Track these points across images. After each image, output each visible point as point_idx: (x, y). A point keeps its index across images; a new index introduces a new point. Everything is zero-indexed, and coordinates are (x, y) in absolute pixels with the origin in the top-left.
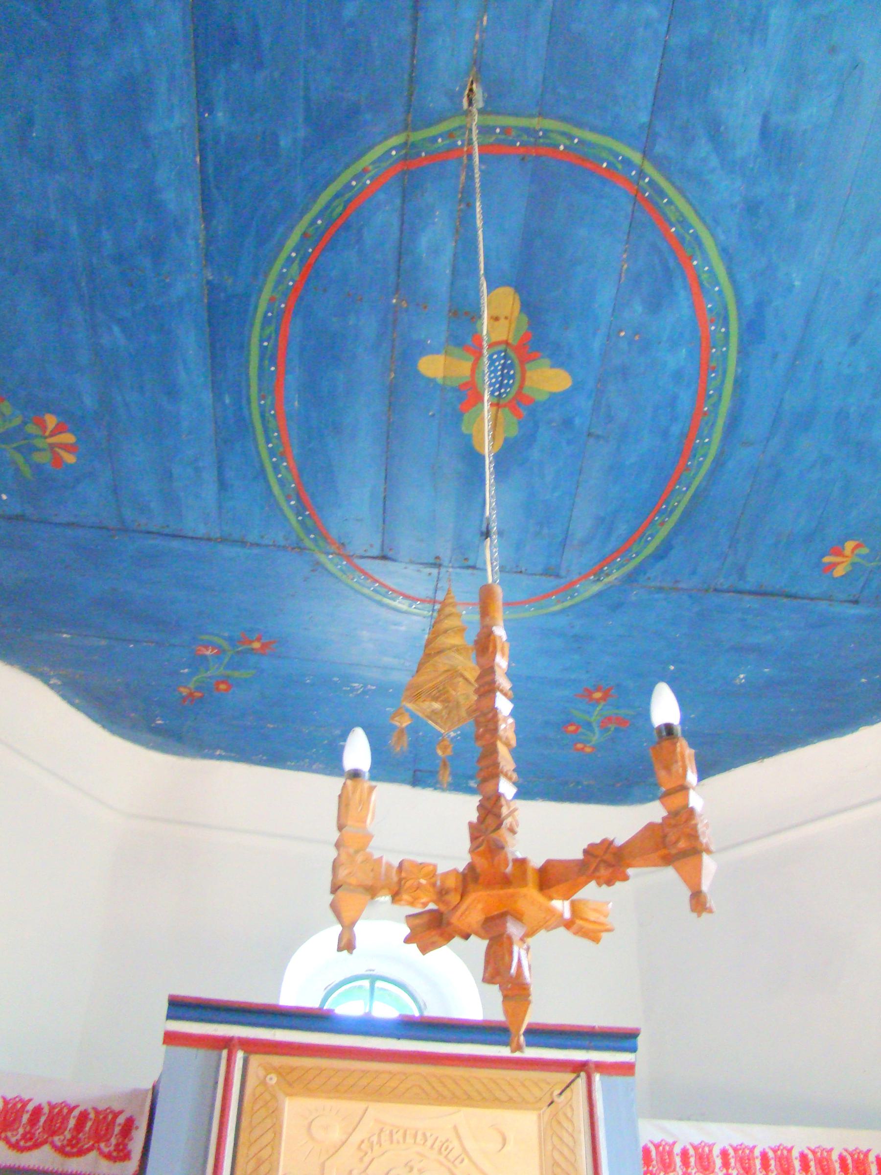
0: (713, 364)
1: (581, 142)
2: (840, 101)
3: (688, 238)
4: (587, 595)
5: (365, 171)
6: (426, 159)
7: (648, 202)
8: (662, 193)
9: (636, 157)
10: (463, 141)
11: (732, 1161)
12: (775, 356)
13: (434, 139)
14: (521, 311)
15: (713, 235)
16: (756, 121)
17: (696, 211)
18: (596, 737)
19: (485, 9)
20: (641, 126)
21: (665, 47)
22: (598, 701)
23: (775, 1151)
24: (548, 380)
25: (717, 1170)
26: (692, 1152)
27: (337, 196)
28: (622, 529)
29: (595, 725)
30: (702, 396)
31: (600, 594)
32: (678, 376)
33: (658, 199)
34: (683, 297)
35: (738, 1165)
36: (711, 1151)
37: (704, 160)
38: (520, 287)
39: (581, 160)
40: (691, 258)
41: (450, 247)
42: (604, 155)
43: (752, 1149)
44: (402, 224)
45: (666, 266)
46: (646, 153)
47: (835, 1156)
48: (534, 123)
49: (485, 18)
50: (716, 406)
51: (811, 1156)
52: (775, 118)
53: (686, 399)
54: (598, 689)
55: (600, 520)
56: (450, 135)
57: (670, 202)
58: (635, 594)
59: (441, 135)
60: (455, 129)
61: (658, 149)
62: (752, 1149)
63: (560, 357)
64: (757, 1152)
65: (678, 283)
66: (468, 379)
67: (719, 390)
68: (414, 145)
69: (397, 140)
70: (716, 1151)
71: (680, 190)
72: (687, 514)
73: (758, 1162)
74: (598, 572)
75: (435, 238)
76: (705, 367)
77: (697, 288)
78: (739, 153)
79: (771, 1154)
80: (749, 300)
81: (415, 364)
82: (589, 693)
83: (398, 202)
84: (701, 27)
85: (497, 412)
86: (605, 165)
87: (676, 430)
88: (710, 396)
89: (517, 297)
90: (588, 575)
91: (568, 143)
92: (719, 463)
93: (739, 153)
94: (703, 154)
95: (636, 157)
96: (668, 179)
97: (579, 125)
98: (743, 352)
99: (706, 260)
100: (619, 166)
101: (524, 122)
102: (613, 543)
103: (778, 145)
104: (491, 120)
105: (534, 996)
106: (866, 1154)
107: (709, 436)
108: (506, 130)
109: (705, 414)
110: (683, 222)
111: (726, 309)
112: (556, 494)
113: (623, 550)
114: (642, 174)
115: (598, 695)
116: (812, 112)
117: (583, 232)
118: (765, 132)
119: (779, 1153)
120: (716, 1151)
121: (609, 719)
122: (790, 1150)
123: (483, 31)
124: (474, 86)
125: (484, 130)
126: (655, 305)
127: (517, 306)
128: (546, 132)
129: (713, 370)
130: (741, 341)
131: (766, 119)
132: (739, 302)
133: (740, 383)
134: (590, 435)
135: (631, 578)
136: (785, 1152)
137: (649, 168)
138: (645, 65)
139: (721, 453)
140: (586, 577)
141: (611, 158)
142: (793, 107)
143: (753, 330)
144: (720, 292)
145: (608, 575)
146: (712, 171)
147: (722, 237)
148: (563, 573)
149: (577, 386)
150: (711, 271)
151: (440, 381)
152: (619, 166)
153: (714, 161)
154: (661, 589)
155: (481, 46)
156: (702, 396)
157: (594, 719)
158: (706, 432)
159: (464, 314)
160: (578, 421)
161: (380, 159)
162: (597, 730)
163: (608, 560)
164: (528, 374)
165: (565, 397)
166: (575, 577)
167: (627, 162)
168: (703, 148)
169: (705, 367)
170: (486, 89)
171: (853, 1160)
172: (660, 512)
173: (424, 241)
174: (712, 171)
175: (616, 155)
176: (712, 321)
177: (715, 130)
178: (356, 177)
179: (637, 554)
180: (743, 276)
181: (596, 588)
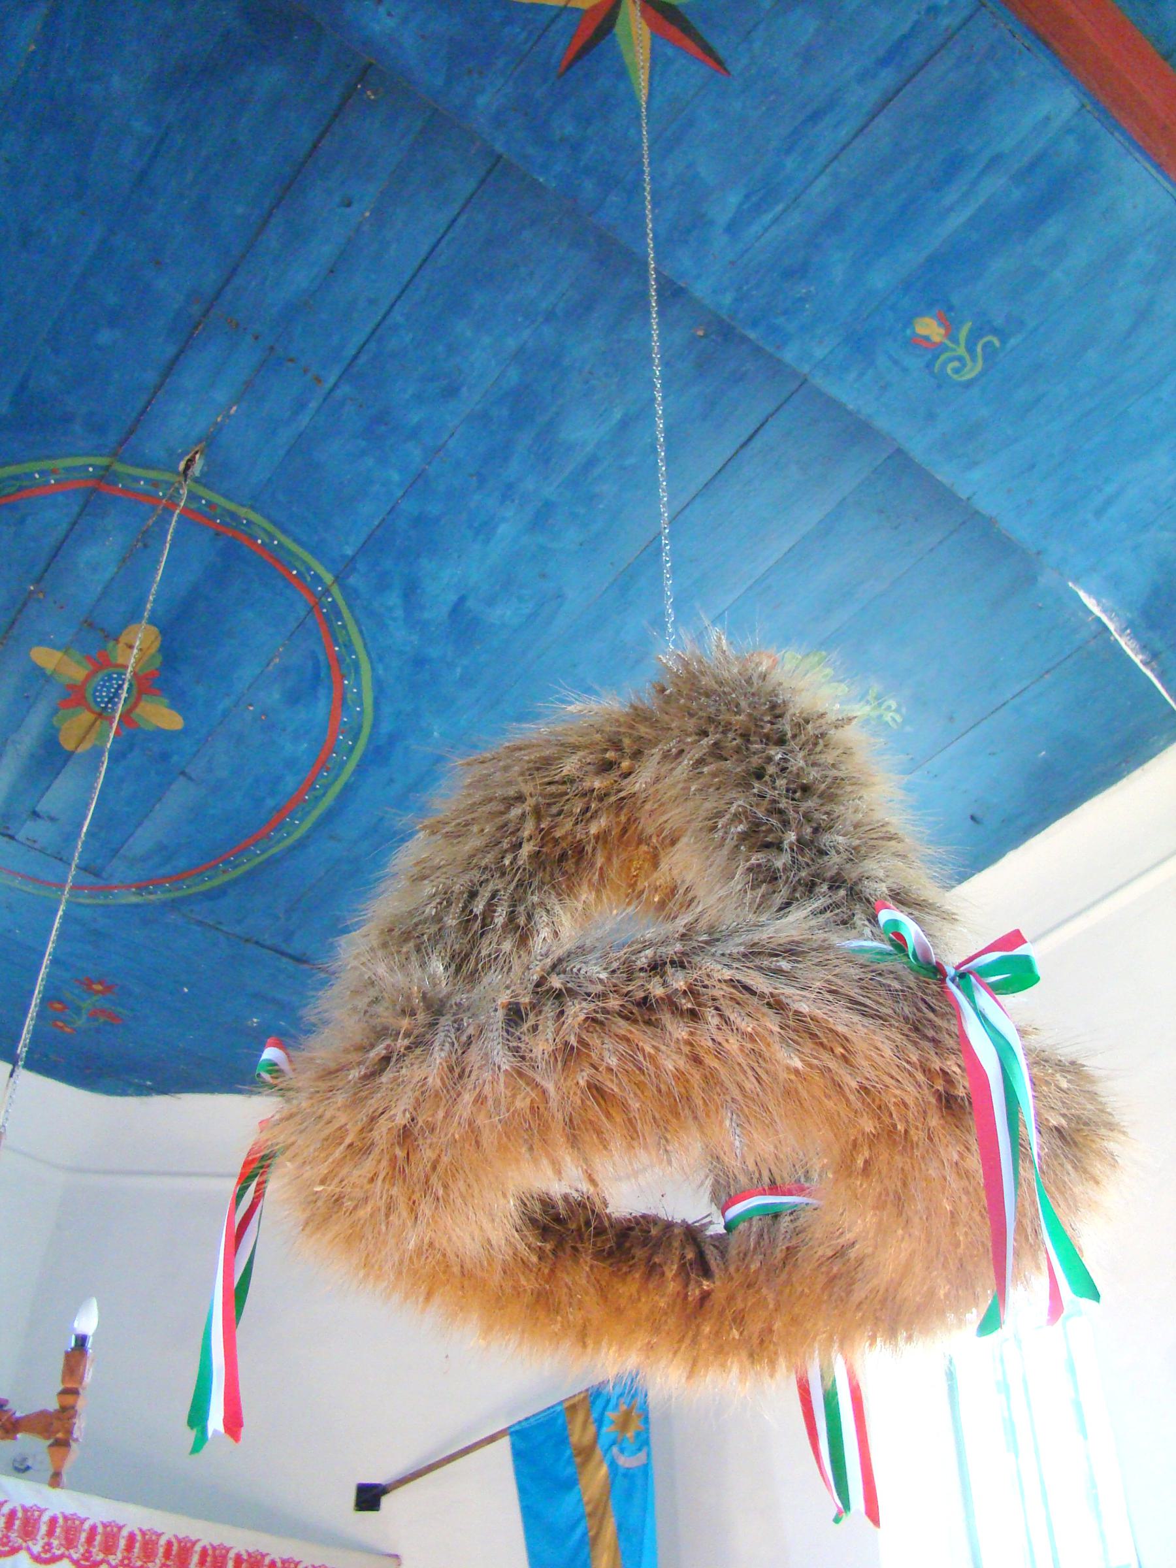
0: (330, 765)
1: (280, 545)
2: (533, 616)
3: (348, 660)
4: (123, 901)
5: (55, 471)
6: (120, 490)
7: (325, 619)
8: (339, 615)
9: (328, 578)
10: (164, 495)
11: (58, 1530)
12: (392, 780)
13: (137, 479)
14: (159, 650)
15: (373, 669)
16: (452, 597)
17: (365, 645)
18: (81, 1022)
19: (238, 400)
20: (343, 556)
21: (393, 508)
22: (97, 992)
23: (105, 1526)
24: (161, 716)
25: (38, 1538)
26: (20, 1514)
27: (16, 478)
28: (182, 863)
29: (83, 1012)
30: (309, 785)
31: (137, 906)
32: (290, 763)
33: (332, 617)
34: (321, 708)
35: (62, 1536)
36: (40, 1516)
37: (390, 609)
38: (163, 632)
39: (277, 561)
40: (343, 677)
41: (112, 569)
42: (298, 564)
43: (83, 1521)
44: (71, 529)
45: (322, 674)
46: (337, 579)
47: (163, 1541)
48: (243, 512)
49: (235, 408)
50: (317, 799)
51: (139, 1537)
52: (470, 603)
53: (291, 783)
54: (101, 983)
55: (162, 847)
56: (155, 484)
57: (344, 627)
58: (172, 918)
59: (145, 479)
60: (162, 481)
61: (352, 580)
62: (83, 1521)
63: (179, 701)
64: (87, 1526)
65: (322, 692)
66: (79, 683)
67: (326, 788)
68: (115, 474)
69: (102, 461)
70: (46, 1518)
71: (357, 622)
72: (251, 875)
73: (83, 1536)
74: (141, 888)
75: (98, 558)
76: (321, 764)
77: (341, 701)
78: (426, 615)
79: (100, 1529)
80: (386, 728)
81: (31, 649)
82: (88, 983)
83: (76, 509)
84: (434, 509)
85: (95, 721)
86: (295, 572)
87: (271, 802)
88: (316, 789)
89: (160, 638)
90: (130, 887)
91: (267, 540)
92: (301, 844)
93: (426, 615)
94: (391, 603)
95: (328, 578)
96: (349, 606)
97: (284, 531)
98: (361, 769)
99: (358, 685)
100: (309, 579)
101: (232, 506)
102: (166, 870)
103: (463, 624)
104: (201, 491)
105: (1092, 1064)
106: (194, 1543)
107: (302, 820)
108: (211, 505)
109: (305, 801)
110: (349, 646)
111: (360, 727)
112: (126, 809)
113: (177, 878)
114: (327, 592)
115: (99, 987)
116: (505, 613)
117: (250, 614)
118: (458, 607)
119: (109, 1529)
120: (46, 1518)
121: (103, 1011)
122: (120, 1528)
123: (229, 417)
124: (197, 456)
125: (192, 497)
126: (294, 698)
127: (157, 644)
128: (250, 523)
129: (328, 770)
130: (364, 757)
131: (462, 600)
132: (375, 725)
133: (348, 789)
134: (183, 773)
135: (173, 905)
136: (115, 1530)
137: (335, 590)
138: (369, 511)
139: (308, 836)
140: (129, 887)
141: (303, 569)
142: (491, 601)
143: (378, 754)
144: (361, 713)
145: (151, 893)
146: (394, 620)
147: (381, 672)
148: (105, 875)
149: (185, 731)
150: (359, 695)
151: (49, 672)
152: (309, 579)
153: (399, 613)
154: (200, 923)
155: (220, 428)
156: (309, 785)
157: (87, 1005)
158: (299, 814)
159: (97, 635)
160: (175, 758)
161: (75, 469)
162: (84, 1016)
163: (157, 882)
164: (142, 704)
165: (173, 735)
166: (115, 882)
167: (317, 578)
168: (393, 599)
169: (321, 764)
170: (208, 463)
171: (179, 1547)
172: (225, 861)
173: (88, 554)
174: (394, 620)
175: (309, 569)
176: (342, 733)
177: (411, 591)
178: (42, 473)
179: (188, 887)
180: (387, 709)
181: (134, 899)
